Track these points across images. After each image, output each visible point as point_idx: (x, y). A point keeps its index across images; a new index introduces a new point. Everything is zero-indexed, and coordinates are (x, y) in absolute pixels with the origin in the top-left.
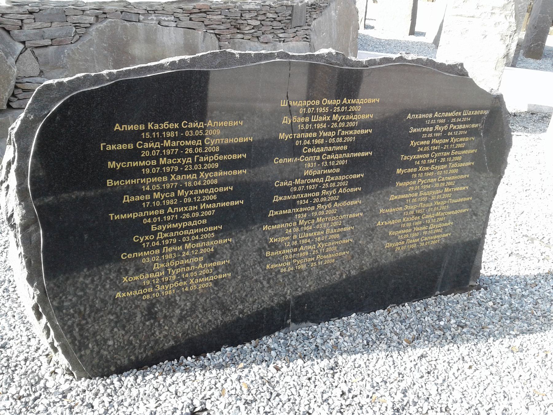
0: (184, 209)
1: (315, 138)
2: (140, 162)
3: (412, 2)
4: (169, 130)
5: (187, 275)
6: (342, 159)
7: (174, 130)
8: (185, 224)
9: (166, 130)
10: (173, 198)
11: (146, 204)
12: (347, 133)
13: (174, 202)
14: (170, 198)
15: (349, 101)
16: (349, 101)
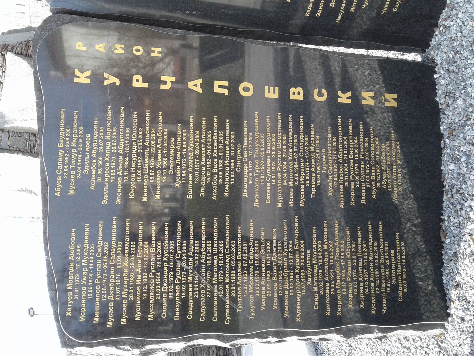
0: (216, 241)
1: (230, 168)
2: (72, 160)
3: (6, 155)
4: (343, 170)
5: (197, 262)
6: (130, 248)
7: (344, 166)
8: (393, 263)
9: (344, 171)
10: (376, 167)
11: (250, 153)
12: (215, 167)
13: (209, 161)
14: (376, 170)
15: (190, 166)
16: (190, 166)
